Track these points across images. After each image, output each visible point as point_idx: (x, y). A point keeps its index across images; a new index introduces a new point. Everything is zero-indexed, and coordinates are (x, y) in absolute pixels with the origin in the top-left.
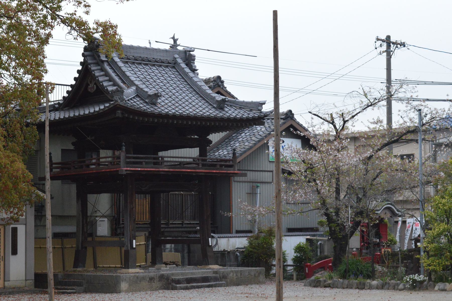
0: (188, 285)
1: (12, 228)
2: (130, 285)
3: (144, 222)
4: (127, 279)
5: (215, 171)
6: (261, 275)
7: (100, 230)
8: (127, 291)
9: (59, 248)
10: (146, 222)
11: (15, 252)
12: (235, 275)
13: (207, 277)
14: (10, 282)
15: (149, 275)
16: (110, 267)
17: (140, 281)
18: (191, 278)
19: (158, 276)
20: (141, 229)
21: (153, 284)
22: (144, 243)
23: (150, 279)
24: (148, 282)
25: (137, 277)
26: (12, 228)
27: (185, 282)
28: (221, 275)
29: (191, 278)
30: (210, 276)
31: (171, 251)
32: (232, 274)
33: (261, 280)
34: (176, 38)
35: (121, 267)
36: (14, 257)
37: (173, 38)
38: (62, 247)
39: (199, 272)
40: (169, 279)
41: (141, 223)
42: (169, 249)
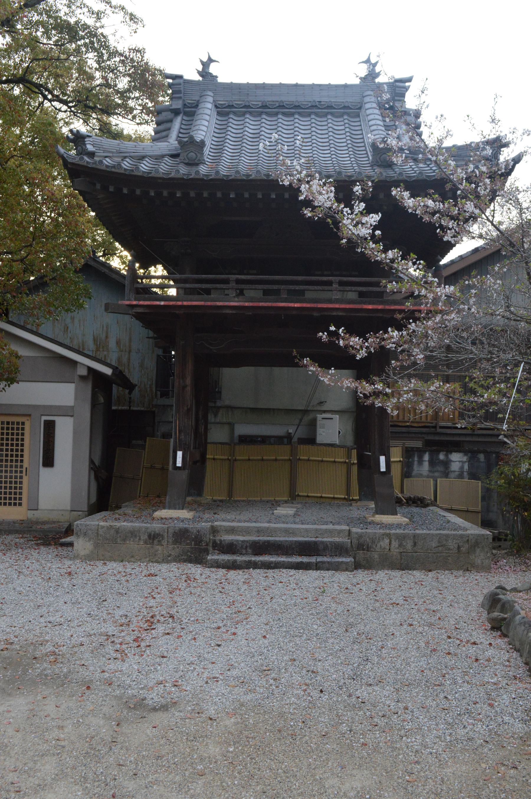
0: (253, 558)
1: (45, 421)
2: (96, 546)
3: (423, 425)
4: (90, 532)
5: (370, 307)
6: (478, 551)
7: (324, 434)
8: (89, 558)
9: (285, 460)
10: (427, 425)
11: (49, 461)
12: (395, 544)
13: (315, 543)
14: (38, 511)
15: (147, 528)
16: (321, 497)
17: (124, 540)
18: (268, 542)
19: (171, 531)
20: (413, 435)
21: (160, 548)
22: (398, 459)
23: (150, 536)
24: (146, 543)
25: (117, 531)
26: (45, 421)
27: (250, 551)
28: (355, 541)
29: (265, 542)
30: (322, 542)
31: (461, 476)
32: (387, 541)
33: (478, 561)
34: (373, 61)
35: (345, 498)
36: (48, 470)
37: (368, 61)
38: (228, 459)
39: (306, 530)
40: (201, 541)
41: (416, 425)
42: (457, 473)
